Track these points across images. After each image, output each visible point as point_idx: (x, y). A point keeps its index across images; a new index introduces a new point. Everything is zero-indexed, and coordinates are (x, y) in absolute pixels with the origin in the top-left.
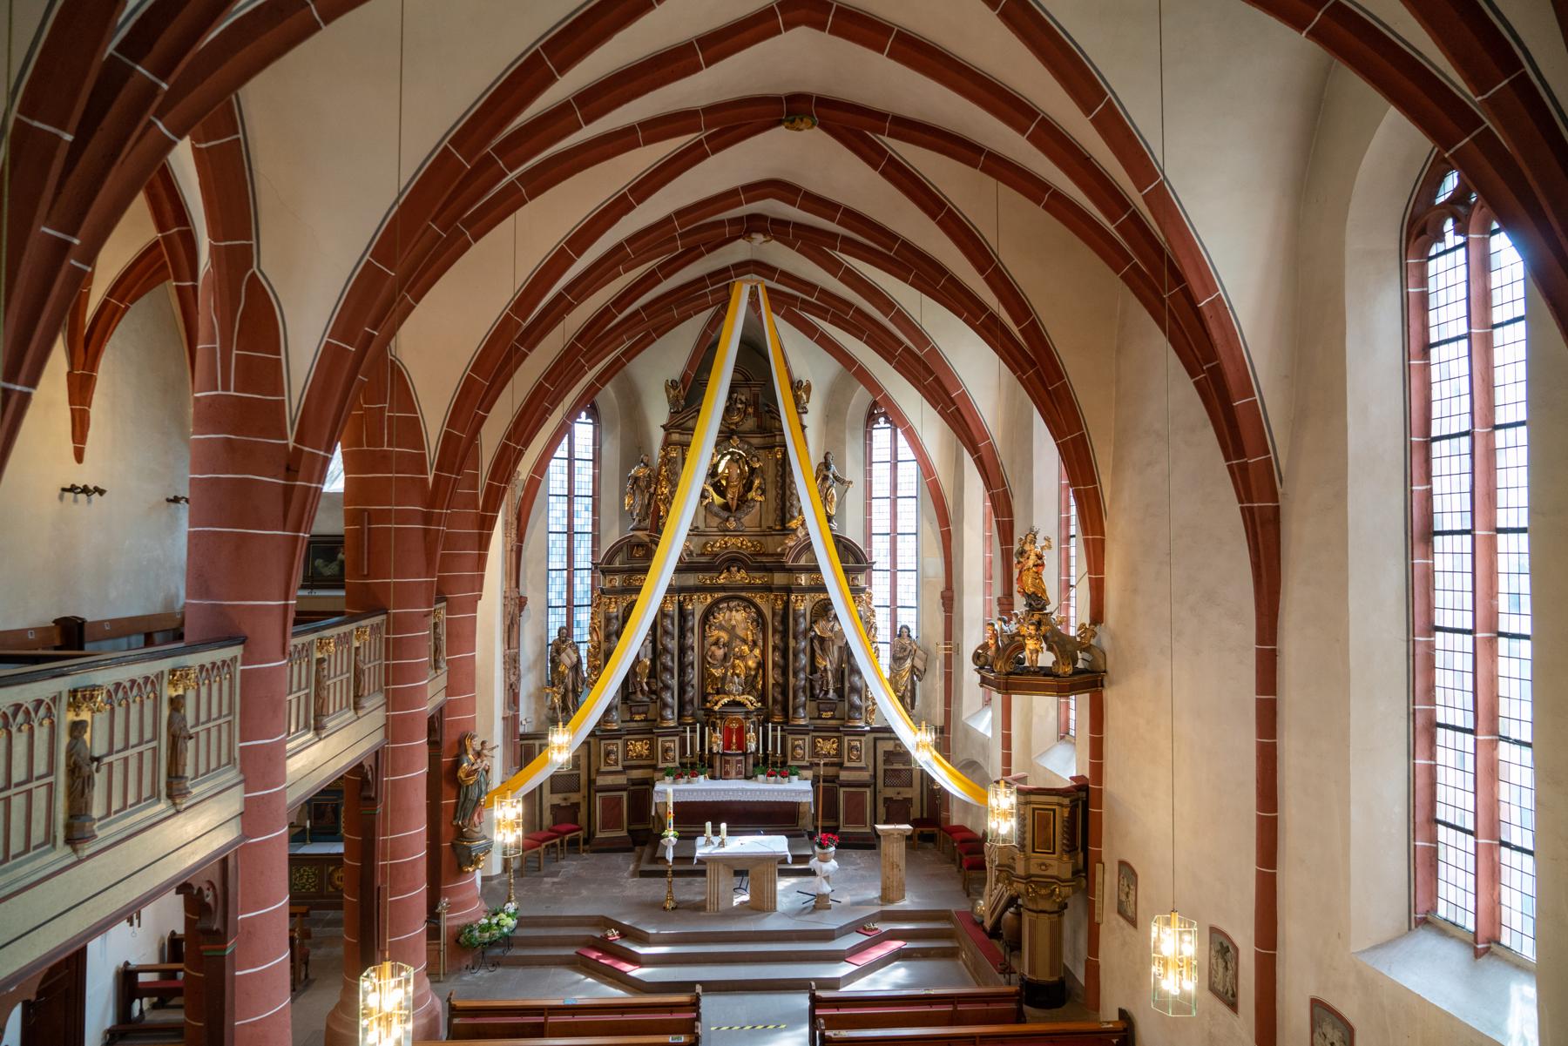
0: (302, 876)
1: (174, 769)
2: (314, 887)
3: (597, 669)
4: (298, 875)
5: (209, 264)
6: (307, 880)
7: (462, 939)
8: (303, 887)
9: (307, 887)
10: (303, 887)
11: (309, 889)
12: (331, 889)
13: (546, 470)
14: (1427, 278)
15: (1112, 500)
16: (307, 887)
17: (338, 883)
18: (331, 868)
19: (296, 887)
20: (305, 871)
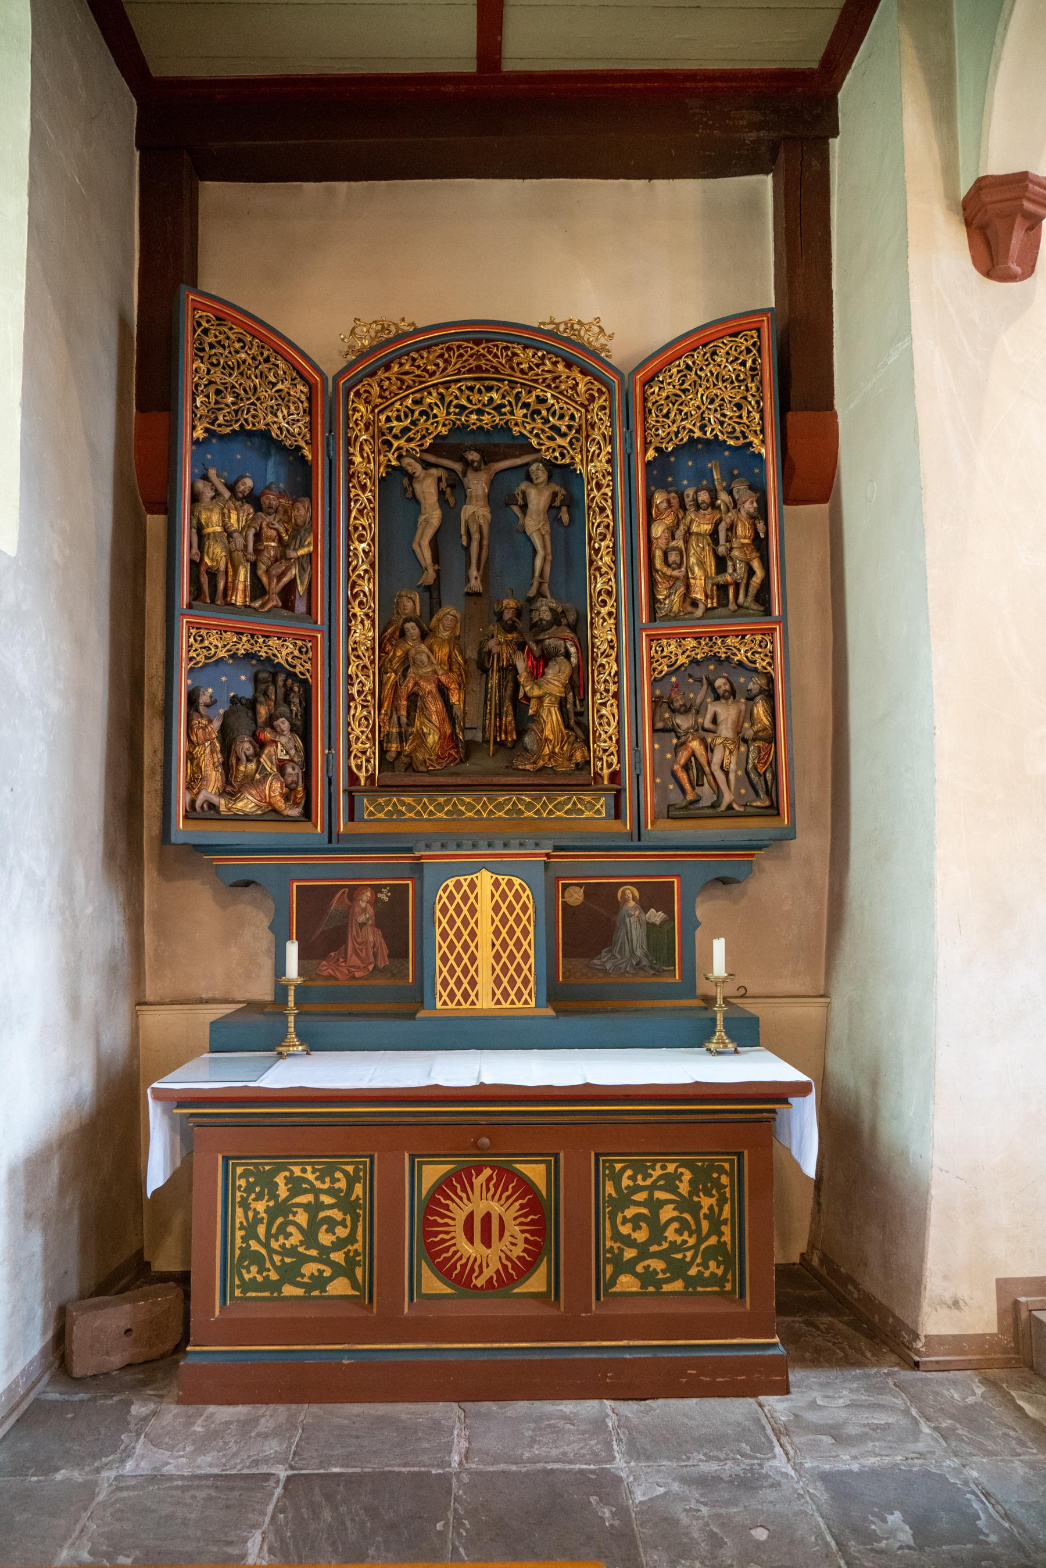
0: (281, 1209)
1: (230, 580)
2: (346, 1271)
3: (727, 536)
4: (261, 1206)
5: (794, 1152)
6: (310, 1236)
7: (1007, 1543)
8: (290, 1274)
9: (310, 1269)
10: (290, 1274)
11: (320, 1282)
12: (432, 1284)
13: (830, 488)
14: (754, 1395)
15: (856, 68)
16: (310, 1269)
17: (468, 1250)
18: (432, 1173)
19: (252, 1273)
20: (296, 1186)
